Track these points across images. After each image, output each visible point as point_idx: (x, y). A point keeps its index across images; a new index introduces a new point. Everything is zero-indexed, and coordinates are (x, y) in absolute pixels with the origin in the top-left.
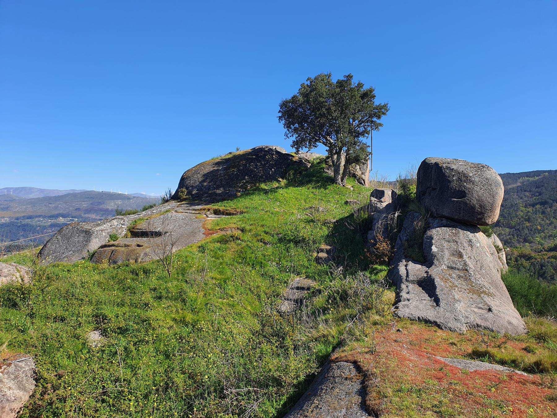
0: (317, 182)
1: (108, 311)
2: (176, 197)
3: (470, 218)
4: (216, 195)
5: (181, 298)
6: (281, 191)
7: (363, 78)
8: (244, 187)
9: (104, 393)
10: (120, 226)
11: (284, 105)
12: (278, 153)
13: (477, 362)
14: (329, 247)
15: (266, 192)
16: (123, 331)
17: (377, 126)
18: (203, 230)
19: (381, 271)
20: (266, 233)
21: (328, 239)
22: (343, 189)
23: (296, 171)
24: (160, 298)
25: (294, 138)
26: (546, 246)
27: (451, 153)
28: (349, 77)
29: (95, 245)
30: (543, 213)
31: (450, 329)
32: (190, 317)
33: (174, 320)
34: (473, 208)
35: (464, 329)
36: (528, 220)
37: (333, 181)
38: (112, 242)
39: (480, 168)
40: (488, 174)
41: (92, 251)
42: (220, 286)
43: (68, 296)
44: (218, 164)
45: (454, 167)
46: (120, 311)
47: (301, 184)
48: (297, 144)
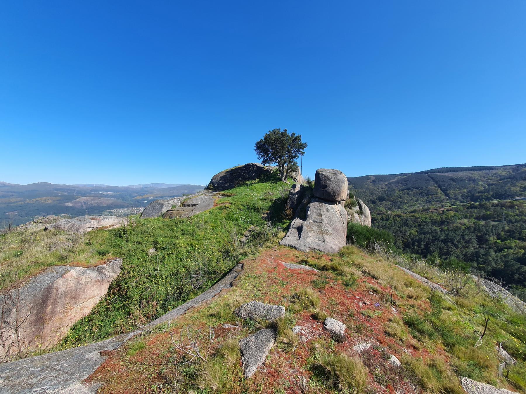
0: (273, 180)
1: (159, 240)
2: (208, 188)
3: (330, 198)
4: (225, 186)
5: (192, 234)
6: (254, 185)
7: (292, 129)
8: (238, 183)
9: (150, 276)
10: (177, 202)
11: (258, 144)
12: (257, 166)
13: (300, 265)
14: (269, 212)
15: (247, 185)
16: (164, 249)
17: (302, 154)
18: (213, 203)
19: (286, 223)
20: (242, 205)
21: (270, 208)
22: (285, 184)
23: (264, 175)
24: (183, 234)
25: (262, 159)
26: (409, 211)
27: (327, 167)
28: (286, 130)
29: (164, 210)
30: (408, 194)
31: (301, 250)
32: (195, 243)
33: (188, 244)
34: (330, 193)
35: (308, 251)
36: (400, 198)
37: (280, 180)
38: (173, 209)
39: (337, 173)
40: (339, 177)
41: (163, 213)
42: (213, 229)
43: (143, 233)
44: (227, 172)
45: (324, 173)
46: (165, 240)
47: (265, 181)
48: (264, 162)
